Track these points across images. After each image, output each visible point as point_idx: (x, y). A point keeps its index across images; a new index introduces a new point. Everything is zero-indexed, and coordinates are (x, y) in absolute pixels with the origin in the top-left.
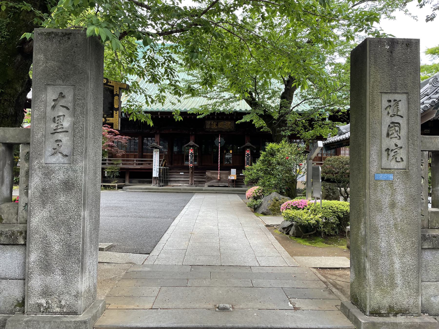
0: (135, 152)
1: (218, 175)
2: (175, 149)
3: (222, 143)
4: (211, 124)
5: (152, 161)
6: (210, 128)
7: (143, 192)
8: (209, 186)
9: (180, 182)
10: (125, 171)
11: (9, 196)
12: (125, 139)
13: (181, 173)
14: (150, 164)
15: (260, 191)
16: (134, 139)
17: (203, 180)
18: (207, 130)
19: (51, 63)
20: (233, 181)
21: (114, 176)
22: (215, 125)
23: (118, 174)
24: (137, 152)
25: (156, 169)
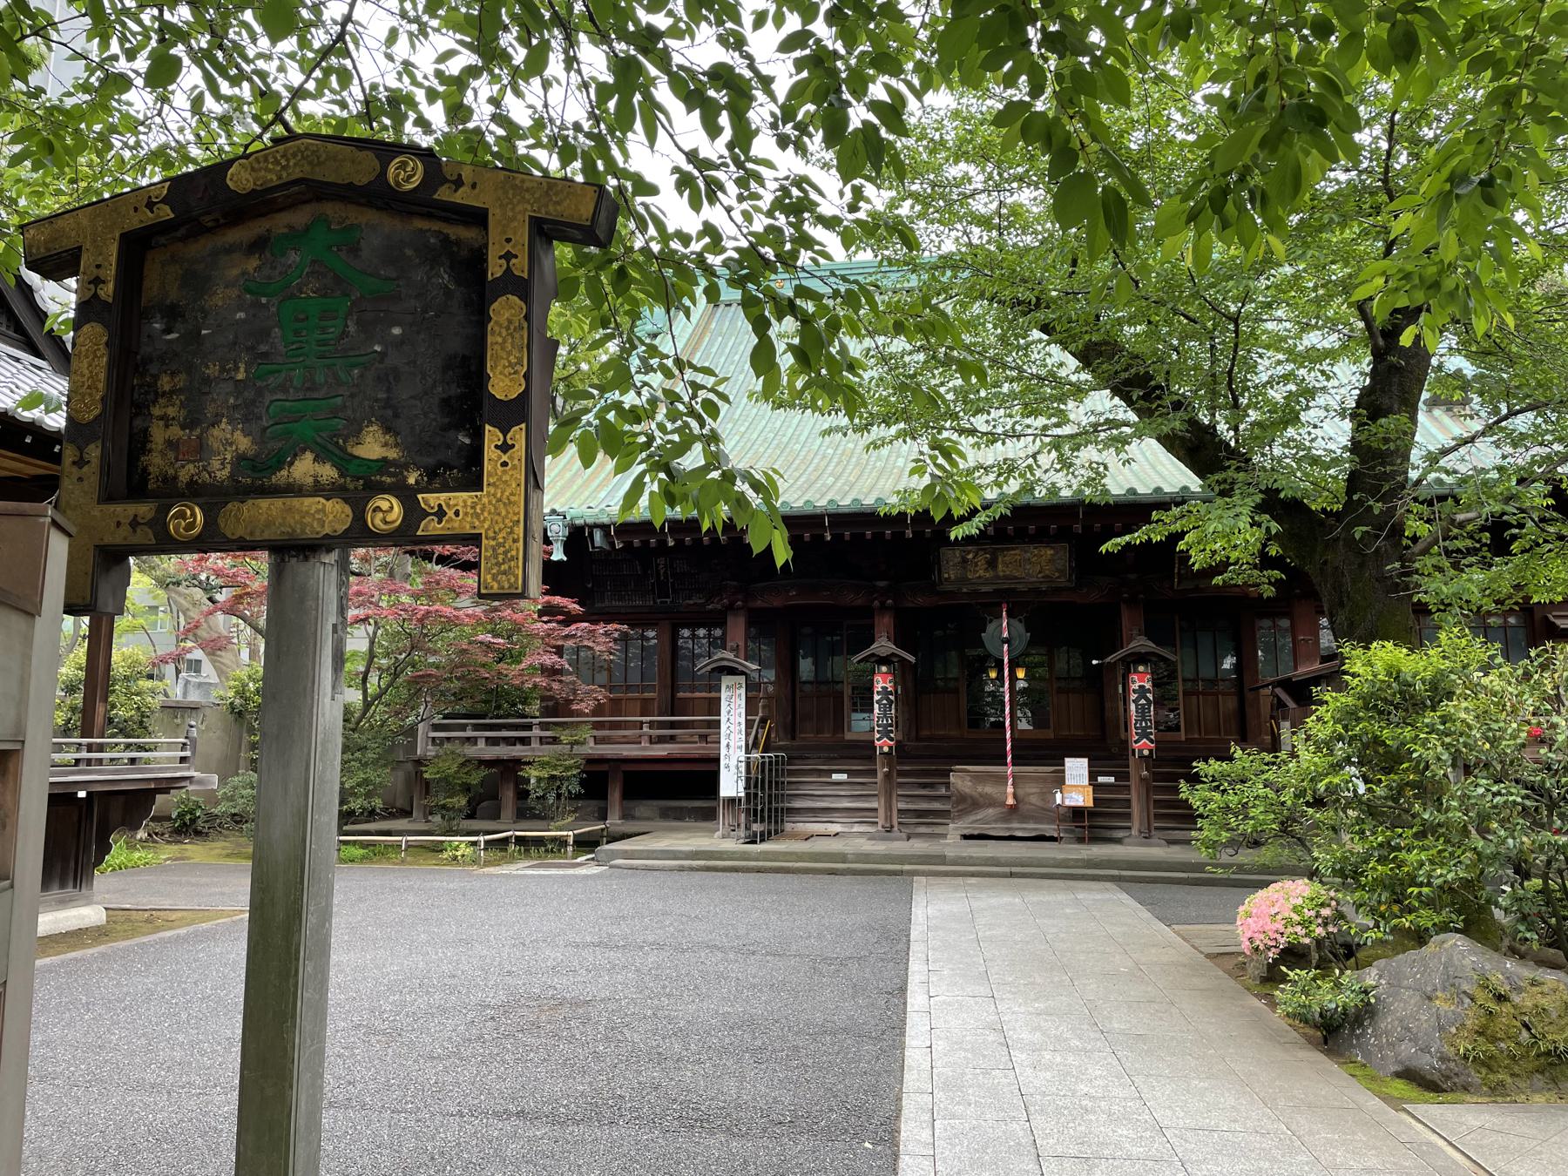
0: (644, 689)
1: (1008, 783)
2: (806, 667)
4: (965, 561)
5: (717, 725)
6: (963, 580)
7: (681, 869)
8: (965, 837)
9: (835, 817)
10: (605, 767)
12: (606, 634)
13: (835, 777)
14: (704, 738)
15: (1326, 912)
16: (644, 638)
17: (936, 806)
18: (949, 588)
20: (1077, 813)
21: (559, 796)
23: (575, 788)
24: (652, 688)
25: (733, 763)
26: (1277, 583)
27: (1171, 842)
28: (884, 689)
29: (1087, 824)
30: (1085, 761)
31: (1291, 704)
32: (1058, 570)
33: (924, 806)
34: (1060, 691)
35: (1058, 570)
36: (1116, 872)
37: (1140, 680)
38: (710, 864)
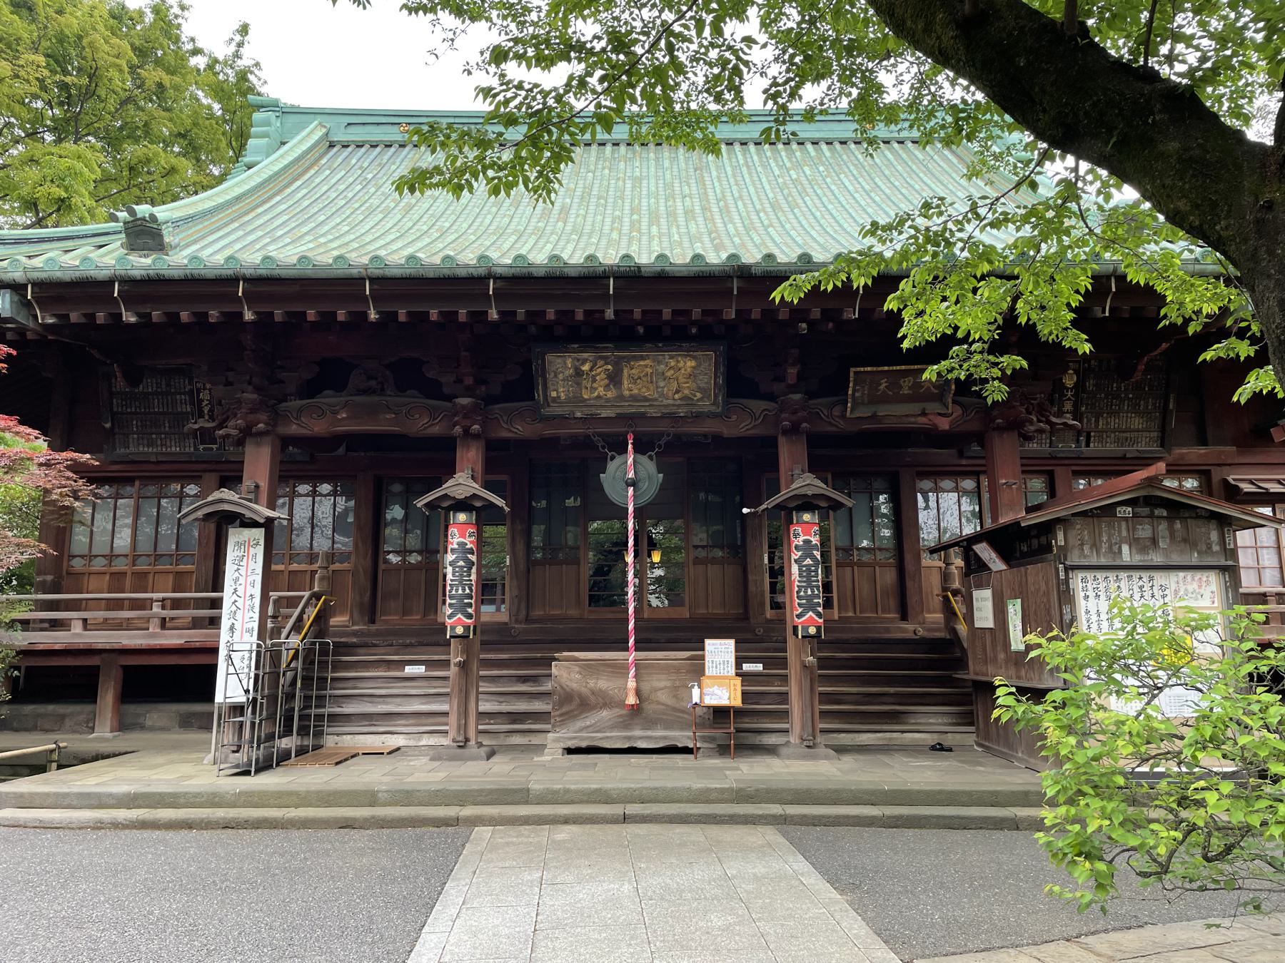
1: (626, 675)
3: (644, 486)
4: (579, 373)
5: (217, 604)
6: (577, 401)
8: (570, 751)
11: (1069, 535)
13: (409, 670)
18: (555, 410)
20: (720, 713)
22: (602, 378)
26: (1012, 379)
27: (841, 750)
28: (462, 545)
29: (733, 731)
30: (732, 642)
31: (997, 564)
32: (700, 389)
33: (522, 706)
34: (697, 561)
35: (700, 389)
36: (776, 809)
37: (805, 533)
38: (156, 816)
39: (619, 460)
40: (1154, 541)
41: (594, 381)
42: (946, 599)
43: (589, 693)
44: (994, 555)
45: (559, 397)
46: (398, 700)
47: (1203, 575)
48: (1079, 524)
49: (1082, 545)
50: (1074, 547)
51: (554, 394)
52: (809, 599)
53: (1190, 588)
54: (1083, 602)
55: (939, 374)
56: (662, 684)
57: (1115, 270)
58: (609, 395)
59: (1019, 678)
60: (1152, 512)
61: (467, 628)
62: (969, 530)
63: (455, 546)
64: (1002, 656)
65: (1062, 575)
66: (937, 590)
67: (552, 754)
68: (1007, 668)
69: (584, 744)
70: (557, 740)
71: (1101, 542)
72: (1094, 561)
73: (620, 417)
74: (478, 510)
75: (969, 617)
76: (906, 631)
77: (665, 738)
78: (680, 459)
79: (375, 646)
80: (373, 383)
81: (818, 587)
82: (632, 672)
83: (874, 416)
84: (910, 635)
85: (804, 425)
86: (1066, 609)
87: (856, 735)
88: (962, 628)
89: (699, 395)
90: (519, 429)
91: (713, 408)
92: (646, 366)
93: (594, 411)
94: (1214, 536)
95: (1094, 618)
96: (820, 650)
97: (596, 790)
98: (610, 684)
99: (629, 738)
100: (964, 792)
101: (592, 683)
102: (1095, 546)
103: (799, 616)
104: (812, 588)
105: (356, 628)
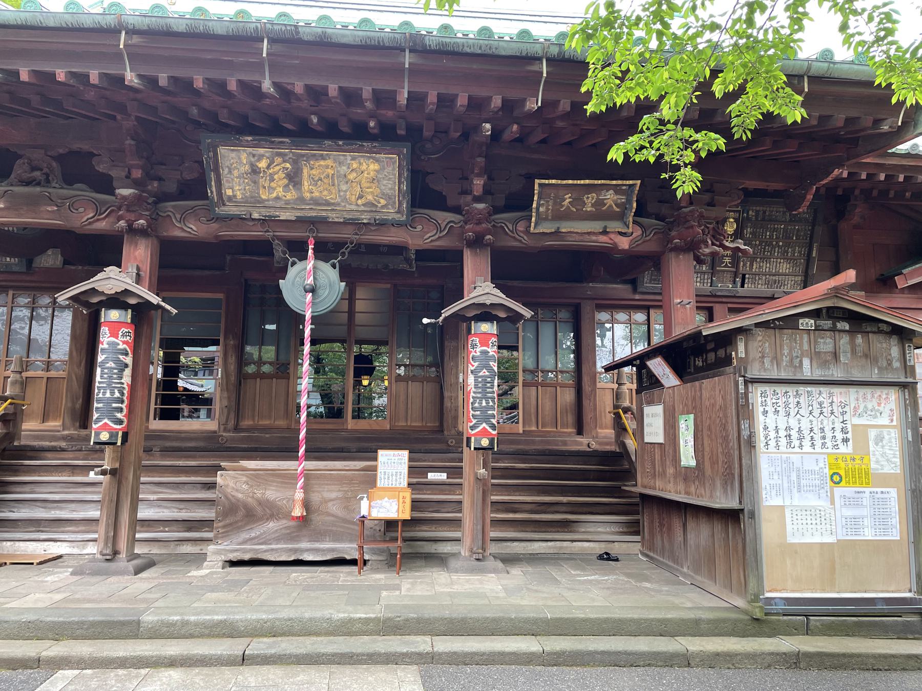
3: (323, 293)
4: (255, 171)
6: (257, 202)
13: (432, 476)
18: (230, 209)
19: (201, 28)
20: (390, 524)
27: (510, 560)
29: (408, 543)
30: (405, 454)
36: (422, 644)
37: (482, 347)
39: (299, 266)
40: (835, 355)
41: (272, 180)
42: (617, 416)
43: (255, 504)
44: (668, 370)
45: (235, 196)
46: (73, 505)
47: (883, 392)
48: (760, 334)
49: (763, 357)
50: (754, 359)
51: (229, 192)
52: (484, 410)
53: (870, 406)
54: (761, 418)
55: (626, 154)
56: (334, 495)
57: (809, 68)
58: (289, 196)
59: (687, 493)
60: (834, 325)
61: (113, 435)
62: (641, 347)
63: (105, 346)
64: (670, 471)
65: (741, 387)
66: (609, 407)
67: (212, 568)
68: (675, 483)
69: (247, 557)
70: (218, 553)
71: (782, 355)
72: (774, 375)
73: (300, 221)
74: (134, 307)
75: (639, 432)
76: (581, 444)
77: (333, 550)
78: (389, 286)
79: (63, 450)
80: (37, 174)
81: (493, 399)
82: (300, 483)
83: (557, 233)
84: (584, 448)
85: (488, 237)
86: (744, 425)
87: (528, 544)
88: (631, 444)
89: (383, 202)
90: (192, 228)
91: (397, 217)
92: (327, 167)
93: (272, 212)
94: (895, 351)
95: (772, 434)
96: (495, 460)
97: (221, 621)
98: (278, 494)
99: (295, 551)
100: (632, 620)
101: (259, 494)
102: (776, 359)
103: (473, 428)
104: (487, 399)
105: (66, 432)
